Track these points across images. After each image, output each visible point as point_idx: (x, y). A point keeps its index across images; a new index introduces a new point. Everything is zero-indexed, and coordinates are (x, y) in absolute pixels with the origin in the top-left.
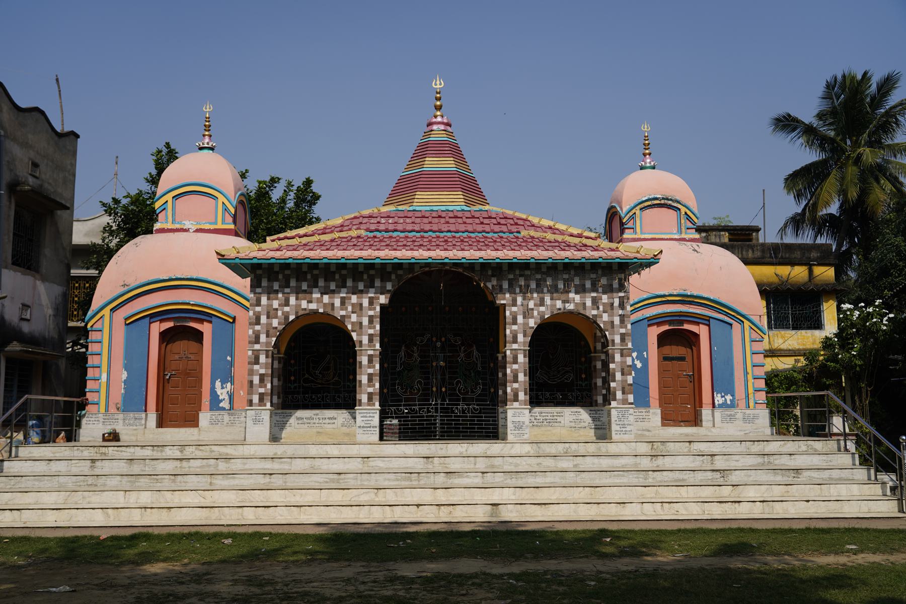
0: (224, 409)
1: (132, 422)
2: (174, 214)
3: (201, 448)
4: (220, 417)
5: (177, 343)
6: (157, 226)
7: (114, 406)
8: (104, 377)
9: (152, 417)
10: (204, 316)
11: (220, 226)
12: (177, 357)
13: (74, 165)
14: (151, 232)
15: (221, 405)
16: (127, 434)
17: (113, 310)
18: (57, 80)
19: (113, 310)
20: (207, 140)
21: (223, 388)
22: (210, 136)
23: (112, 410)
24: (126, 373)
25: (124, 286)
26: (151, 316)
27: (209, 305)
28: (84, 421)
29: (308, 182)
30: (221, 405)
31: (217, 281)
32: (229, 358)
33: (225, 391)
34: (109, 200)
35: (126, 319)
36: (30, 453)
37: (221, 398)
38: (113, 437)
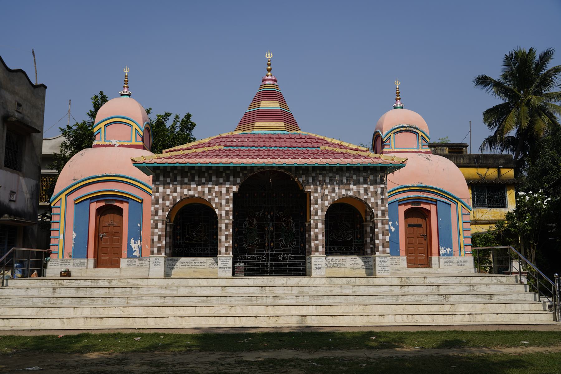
0: (135, 256)
2: (105, 136)
3: (121, 280)
4: (133, 262)
5: (107, 216)
6: (95, 143)
8: (61, 236)
9: (91, 262)
10: (124, 199)
11: (134, 143)
14: (91, 147)
15: (134, 254)
16: (75, 272)
17: (67, 195)
18: (33, 52)
19: (67, 195)
20: (126, 90)
21: (135, 243)
22: (128, 87)
23: (66, 257)
25: (74, 180)
27: (127, 192)
28: (49, 264)
30: (134, 254)
32: (139, 225)
33: (136, 245)
34: (65, 127)
36: (15, 283)
37: (134, 249)
38: (67, 274)
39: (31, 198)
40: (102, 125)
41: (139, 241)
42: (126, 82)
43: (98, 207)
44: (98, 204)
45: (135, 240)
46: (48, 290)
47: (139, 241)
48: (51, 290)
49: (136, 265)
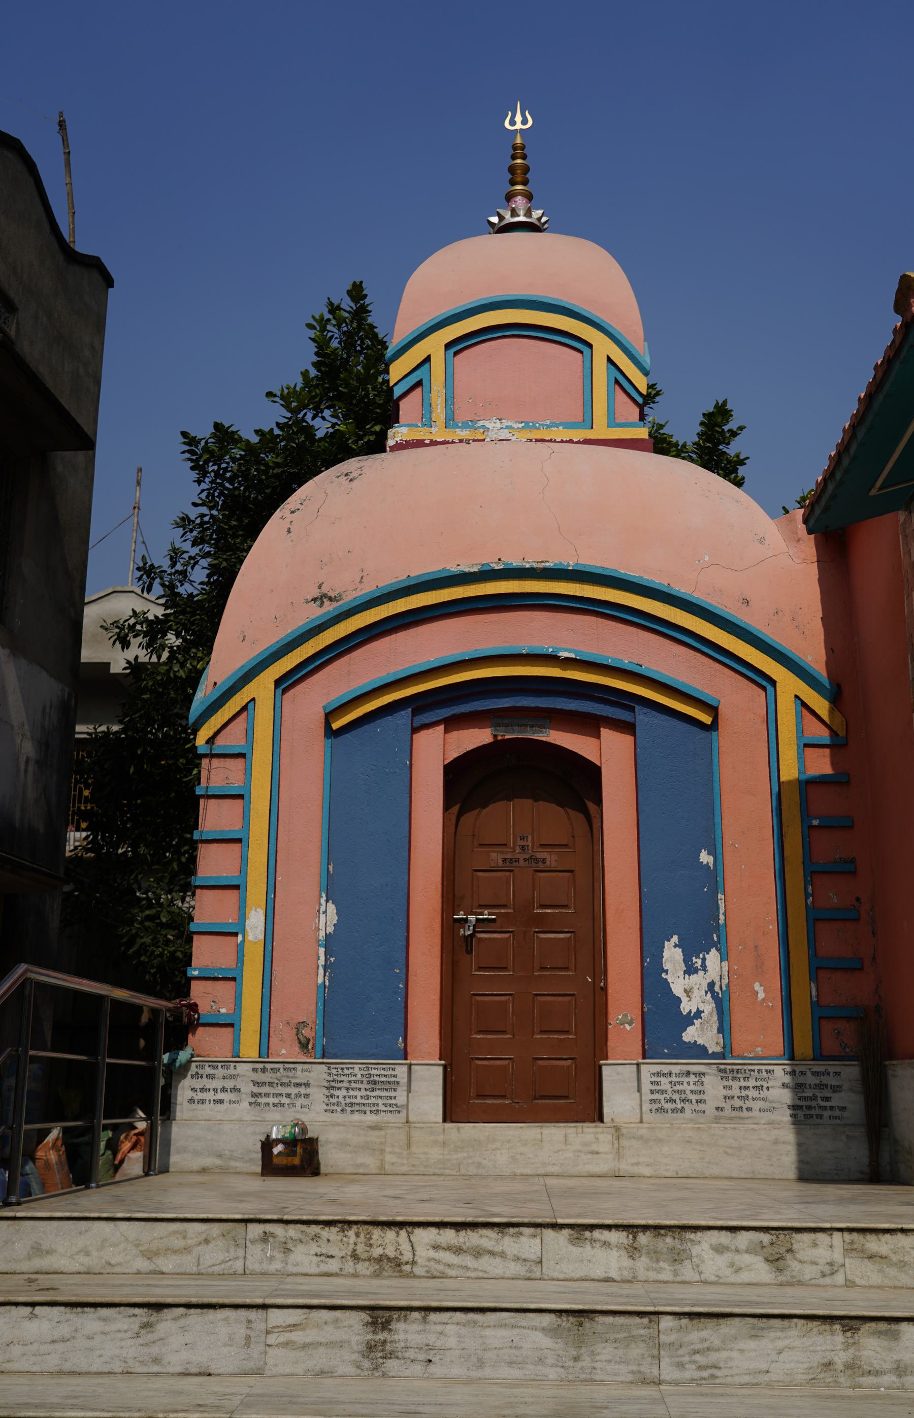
0: (698, 1051)
1: (358, 1095)
2: (450, 400)
3: (873, 1244)
4: (688, 1085)
5: (496, 809)
6: (397, 434)
7: (289, 1035)
8: (255, 921)
10: (605, 703)
11: (601, 431)
13: (97, 353)
14: (384, 451)
15: (691, 1034)
16: (343, 1144)
17: (285, 683)
18: (62, 124)
19: (285, 683)
20: (520, 202)
21: (690, 970)
22: (529, 197)
23: (285, 1049)
25: (320, 599)
27: (626, 662)
28: (184, 1091)
30: (691, 1034)
31: (657, 580)
33: (699, 981)
35: (330, 716)
36: (38, 1250)
38: (296, 1157)
39: (37, 762)
40: (434, 345)
41: (713, 958)
43: (453, 755)
44: (455, 735)
45: (692, 951)
47: (713, 958)
49: (710, 1108)
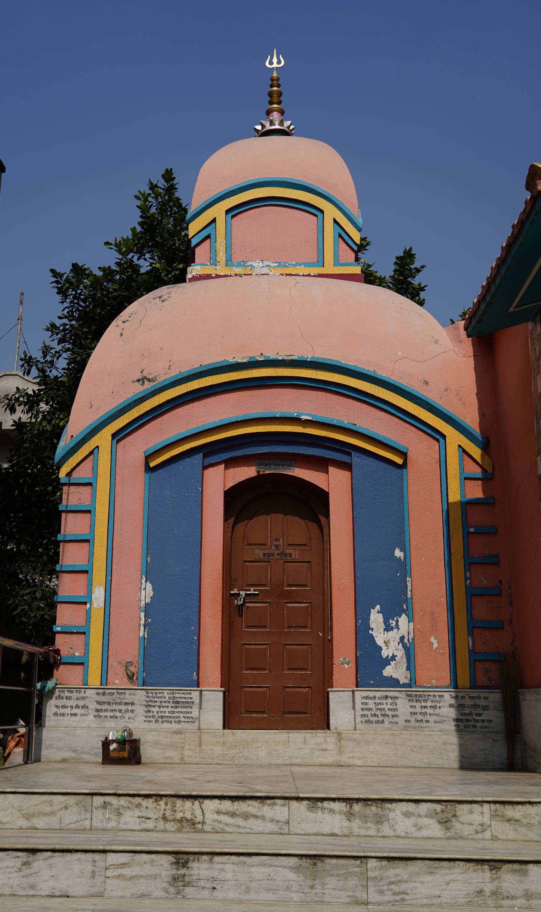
0: (393, 683)
2: (229, 248)
4: (387, 705)
6: (194, 270)
7: (121, 670)
8: (98, 595)
9: (211, 704)
11: (330, 268)
12: (259, 553)
14: (185, 281)
15: (388, 671)
16: (157, 744)
17: (118, 436)
19: (118, 436)
20: (276, 116)
21: (388, 628)
23: (118, 680)
24: (149, 586)
25: (142, 380)
26: (208, 450)
27: (346, 423)
28: (51, 707)
29: (411, 249)
30: (388, 671)
32: (398, 553)
33: (394, 635)
34: (66, 269)
35: (148, 458)
37: (386, 653)
38: (125, 752)
41: (403, 620)
42: (275, 98)
43: (230, 484)
44: (231, 471)
45: (390, 615)
46: (144, 865)
47: (403, 620)
48: (164, 866)
49: (401, 720)
